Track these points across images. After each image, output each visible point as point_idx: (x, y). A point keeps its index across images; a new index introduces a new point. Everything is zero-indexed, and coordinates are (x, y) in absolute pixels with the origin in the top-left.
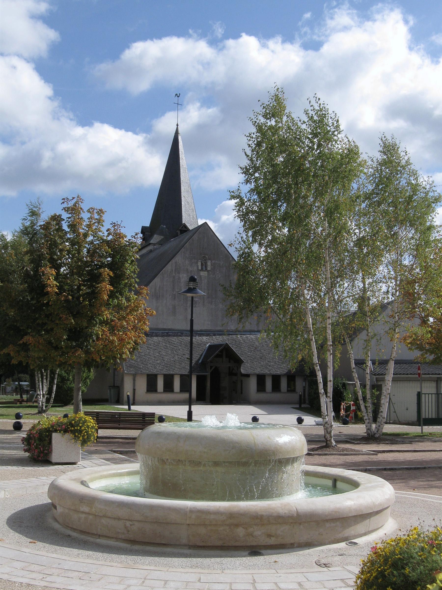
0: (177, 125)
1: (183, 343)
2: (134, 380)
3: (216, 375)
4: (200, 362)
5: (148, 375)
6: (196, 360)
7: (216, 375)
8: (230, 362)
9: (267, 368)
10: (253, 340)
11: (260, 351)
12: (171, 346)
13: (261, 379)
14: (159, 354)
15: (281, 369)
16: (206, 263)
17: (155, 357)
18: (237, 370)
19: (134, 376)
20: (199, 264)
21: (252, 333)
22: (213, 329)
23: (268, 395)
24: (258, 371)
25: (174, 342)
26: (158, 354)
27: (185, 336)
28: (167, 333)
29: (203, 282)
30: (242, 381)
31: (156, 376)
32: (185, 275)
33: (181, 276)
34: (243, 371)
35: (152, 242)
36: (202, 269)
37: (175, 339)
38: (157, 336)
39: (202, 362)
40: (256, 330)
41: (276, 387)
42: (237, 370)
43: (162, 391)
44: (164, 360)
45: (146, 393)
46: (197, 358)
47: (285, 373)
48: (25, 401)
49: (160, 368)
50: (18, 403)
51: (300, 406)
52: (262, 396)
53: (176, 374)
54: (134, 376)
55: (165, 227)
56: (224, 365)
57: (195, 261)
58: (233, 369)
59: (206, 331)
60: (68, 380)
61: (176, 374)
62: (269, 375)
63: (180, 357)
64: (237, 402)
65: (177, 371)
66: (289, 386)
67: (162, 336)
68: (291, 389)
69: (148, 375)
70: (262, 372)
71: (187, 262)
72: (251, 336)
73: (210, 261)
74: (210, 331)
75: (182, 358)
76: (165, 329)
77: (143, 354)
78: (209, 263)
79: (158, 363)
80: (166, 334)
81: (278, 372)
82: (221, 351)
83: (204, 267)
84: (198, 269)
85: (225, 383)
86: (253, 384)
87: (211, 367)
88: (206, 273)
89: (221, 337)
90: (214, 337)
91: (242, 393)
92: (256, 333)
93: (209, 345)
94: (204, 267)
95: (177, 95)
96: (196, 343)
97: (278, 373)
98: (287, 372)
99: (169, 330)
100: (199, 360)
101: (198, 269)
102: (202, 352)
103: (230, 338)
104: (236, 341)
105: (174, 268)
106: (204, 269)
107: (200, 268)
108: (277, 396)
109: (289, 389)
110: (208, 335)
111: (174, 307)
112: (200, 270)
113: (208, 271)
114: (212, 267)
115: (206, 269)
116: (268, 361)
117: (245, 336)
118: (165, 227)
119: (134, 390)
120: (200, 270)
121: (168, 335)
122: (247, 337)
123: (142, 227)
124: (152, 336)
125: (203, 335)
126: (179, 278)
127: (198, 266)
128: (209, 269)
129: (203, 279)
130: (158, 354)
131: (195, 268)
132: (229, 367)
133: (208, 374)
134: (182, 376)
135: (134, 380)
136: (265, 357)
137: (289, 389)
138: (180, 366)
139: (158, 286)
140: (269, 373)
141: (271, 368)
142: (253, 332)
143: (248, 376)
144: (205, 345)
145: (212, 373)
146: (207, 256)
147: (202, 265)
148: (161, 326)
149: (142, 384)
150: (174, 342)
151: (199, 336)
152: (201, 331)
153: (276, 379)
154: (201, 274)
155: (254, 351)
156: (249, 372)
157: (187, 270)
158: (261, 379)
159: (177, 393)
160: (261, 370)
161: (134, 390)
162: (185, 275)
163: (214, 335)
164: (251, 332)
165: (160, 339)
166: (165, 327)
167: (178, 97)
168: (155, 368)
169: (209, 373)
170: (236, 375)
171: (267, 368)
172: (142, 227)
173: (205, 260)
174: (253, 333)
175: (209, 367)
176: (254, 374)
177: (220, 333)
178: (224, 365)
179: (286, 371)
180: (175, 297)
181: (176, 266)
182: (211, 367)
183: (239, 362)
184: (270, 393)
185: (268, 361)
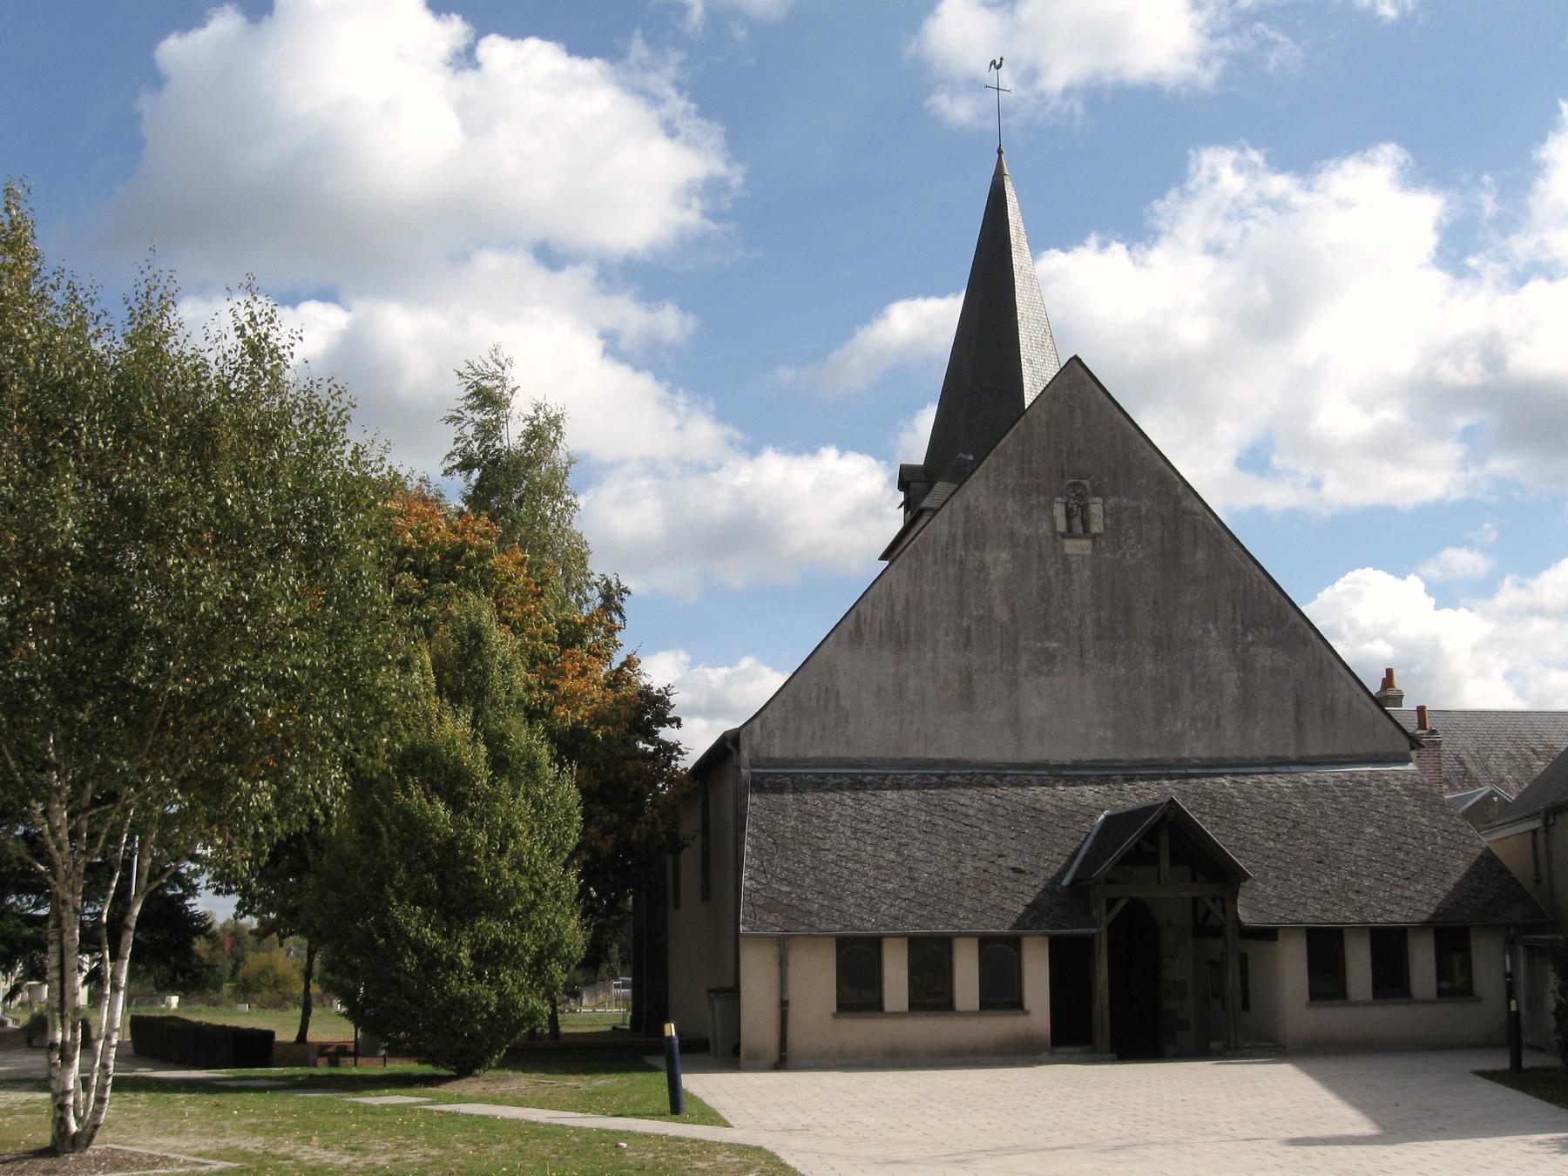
0: (1000, 152)
1: (1000, 811)
2: (783, 963)
3: (1136, 933)
4: (1065, 882)
5: (843, 943)
6: (1050, 875)
7: (1136, 933)
8: (1194, 880)
9: (1347, 900)
10: (1283, 795)
11: (1316, 834)
12: (953, 825)
13: (1325, 948)
14: (899, 853)
15: (1413, 902)
16: (1084, 508)
17: (878, 867)
18: (1224, 911)
19: (782, 945)
20: (1059, 511)
21: (1277, 769)
22: (1123, 756)
23: (1361, 1011)
24: (1313, 913)
25: (964, 810)
26: (892, 856)
27: (1013, 785)
28: (941, 777)
29: (1076, 577)
30: (1244, 958)
31: (874, 945)
32: (1004, 555)
33: (989, 557)
34: (1245, 916)
35: (925, 504)
36: (1070, 528)
37: (968, 799)
38: (898, 787)
39: (1073, 882)
40: (1292, 753)
41: (1390, 980)
42: (1224, 911)
43: (905, 1007)
44: (913, 879)
45: (835, 1016)
46: (1056, 868)
47: (1424, 917)
48: (350, 1054)
49: (894, 911)
50: (322, 1061)
51: (1516, 1060)
52: (1333, 1018)
53: (960, 935)
54: (782, 945)
55: (971, 457)
56: (1169, 893)
57: (1043, 499)
58: (1209, 912)
59: (1096, 764)
60: (453, 964)
61: (960, 935)
62: (1358, 929)
63: (984, 864)
64: (1228, 1047)
65: (963, 921)
66: (1442, 972)
67: (921, 786)
68: (1455, 983)
69: (843, 943)
70: (1330, 918)
71: (1010, 506)
72: (1276, 779)
73: (1099, 499)
74: (1110, 764)
75: (993, 869)
76: (935, 764)
77: (831, 857)
78: (1096, 509)
79: (886, 892)
80: (935, 779)
81: (1398, 917)
82: (1151, 836)
83: (1078, 519)
84: (1054, 531)
85: (1180, 967)
86: (1290, 968)
87: (1111, 903)
88: (1086, 543)
89: (1154, 785)
90: (1127, 787)
91: (1246, 1006)
92: (1293, 769)
93: (1107, 817)
94: (1078, 519)
95: (993, 62)
96: (1053, 810)
97: (1396, 918)
98: (1435, 915)
99: (952, 763)
100: (1061, 874)
101: (1054, 531)
102: (1076, 845)
103: (1189, 789)
104: (1214, 800)
105: (960, 531)
106: (1079, 529)
107: (1061, 526)
108: (1392, 1017)
109: (1445, 985)
110: (1101, 780)
111: (967, 677)
112: (1063, 536)
113: (1094, 537)
114: (1108, 520)
115: (1086, 530)
116: (1351, 874)
117: (1249, 781)
118: (971, 457)
119: (784, 1004)
120: (1063, 536)
121: (944, 783)
122: (1259, 785)
123: (902, 468)
124: (879, 788)
125: (1086, 780)
126: (982, 567)
127: (1053, 521)
128: (1096, 528)
129: (1074, 566)
130: (892, 856)
131: (1045, 527)
132: (1195, 900)
133: (1099, 931)
134: (986, 943)
135: (783, 963)
136: (1337, 858)
137: (1445, 985)
138: (980, 902)
139: (902, 598)
140: (1356, 919)
141: (1364, 899)
142: (1281, 764)
143: (1268, 934)
144: (1092, 816)
145: (1112, 929)
146: (1086, 483)
147: (1069, 515)
148: (915, 751)
149: (816, 978)
150: (964, 810)
151: (1065, 785)
152: (1076, 765)
153: (1389, 945)
154: (1068, 551)
155: (1291, 837)
156: (1273, 918)
157: (1012, 534)
158: (1325, 948)
159: (968, 1014)
160: (1325, 911)
161: (784, 1004)
162: (1004, 555)
163: (1130, 779)
164: (1274, 763)
165: (910, 796)
166: (932, 755)
167: (998, 67)
168: (874, 911)
169: (1103, 929)
170: (1218, 932)
171: (1347, 900)
172: (902, 468)
173: (1080, 497)
174: (1284, 769)
175: (1104, 903)
176: (1296, 928)
177: (1154, 770)
178: (1169, 893)
179: (1425, 911)
180: (968, 640)
181: (967, 522)
182: (1111, 903)
183: (1223, 875)
184: (1366, 1004)
185: (1351, 874)
